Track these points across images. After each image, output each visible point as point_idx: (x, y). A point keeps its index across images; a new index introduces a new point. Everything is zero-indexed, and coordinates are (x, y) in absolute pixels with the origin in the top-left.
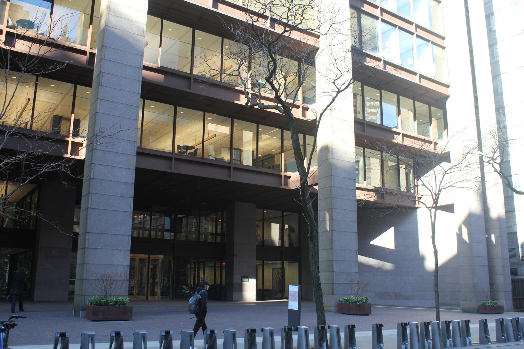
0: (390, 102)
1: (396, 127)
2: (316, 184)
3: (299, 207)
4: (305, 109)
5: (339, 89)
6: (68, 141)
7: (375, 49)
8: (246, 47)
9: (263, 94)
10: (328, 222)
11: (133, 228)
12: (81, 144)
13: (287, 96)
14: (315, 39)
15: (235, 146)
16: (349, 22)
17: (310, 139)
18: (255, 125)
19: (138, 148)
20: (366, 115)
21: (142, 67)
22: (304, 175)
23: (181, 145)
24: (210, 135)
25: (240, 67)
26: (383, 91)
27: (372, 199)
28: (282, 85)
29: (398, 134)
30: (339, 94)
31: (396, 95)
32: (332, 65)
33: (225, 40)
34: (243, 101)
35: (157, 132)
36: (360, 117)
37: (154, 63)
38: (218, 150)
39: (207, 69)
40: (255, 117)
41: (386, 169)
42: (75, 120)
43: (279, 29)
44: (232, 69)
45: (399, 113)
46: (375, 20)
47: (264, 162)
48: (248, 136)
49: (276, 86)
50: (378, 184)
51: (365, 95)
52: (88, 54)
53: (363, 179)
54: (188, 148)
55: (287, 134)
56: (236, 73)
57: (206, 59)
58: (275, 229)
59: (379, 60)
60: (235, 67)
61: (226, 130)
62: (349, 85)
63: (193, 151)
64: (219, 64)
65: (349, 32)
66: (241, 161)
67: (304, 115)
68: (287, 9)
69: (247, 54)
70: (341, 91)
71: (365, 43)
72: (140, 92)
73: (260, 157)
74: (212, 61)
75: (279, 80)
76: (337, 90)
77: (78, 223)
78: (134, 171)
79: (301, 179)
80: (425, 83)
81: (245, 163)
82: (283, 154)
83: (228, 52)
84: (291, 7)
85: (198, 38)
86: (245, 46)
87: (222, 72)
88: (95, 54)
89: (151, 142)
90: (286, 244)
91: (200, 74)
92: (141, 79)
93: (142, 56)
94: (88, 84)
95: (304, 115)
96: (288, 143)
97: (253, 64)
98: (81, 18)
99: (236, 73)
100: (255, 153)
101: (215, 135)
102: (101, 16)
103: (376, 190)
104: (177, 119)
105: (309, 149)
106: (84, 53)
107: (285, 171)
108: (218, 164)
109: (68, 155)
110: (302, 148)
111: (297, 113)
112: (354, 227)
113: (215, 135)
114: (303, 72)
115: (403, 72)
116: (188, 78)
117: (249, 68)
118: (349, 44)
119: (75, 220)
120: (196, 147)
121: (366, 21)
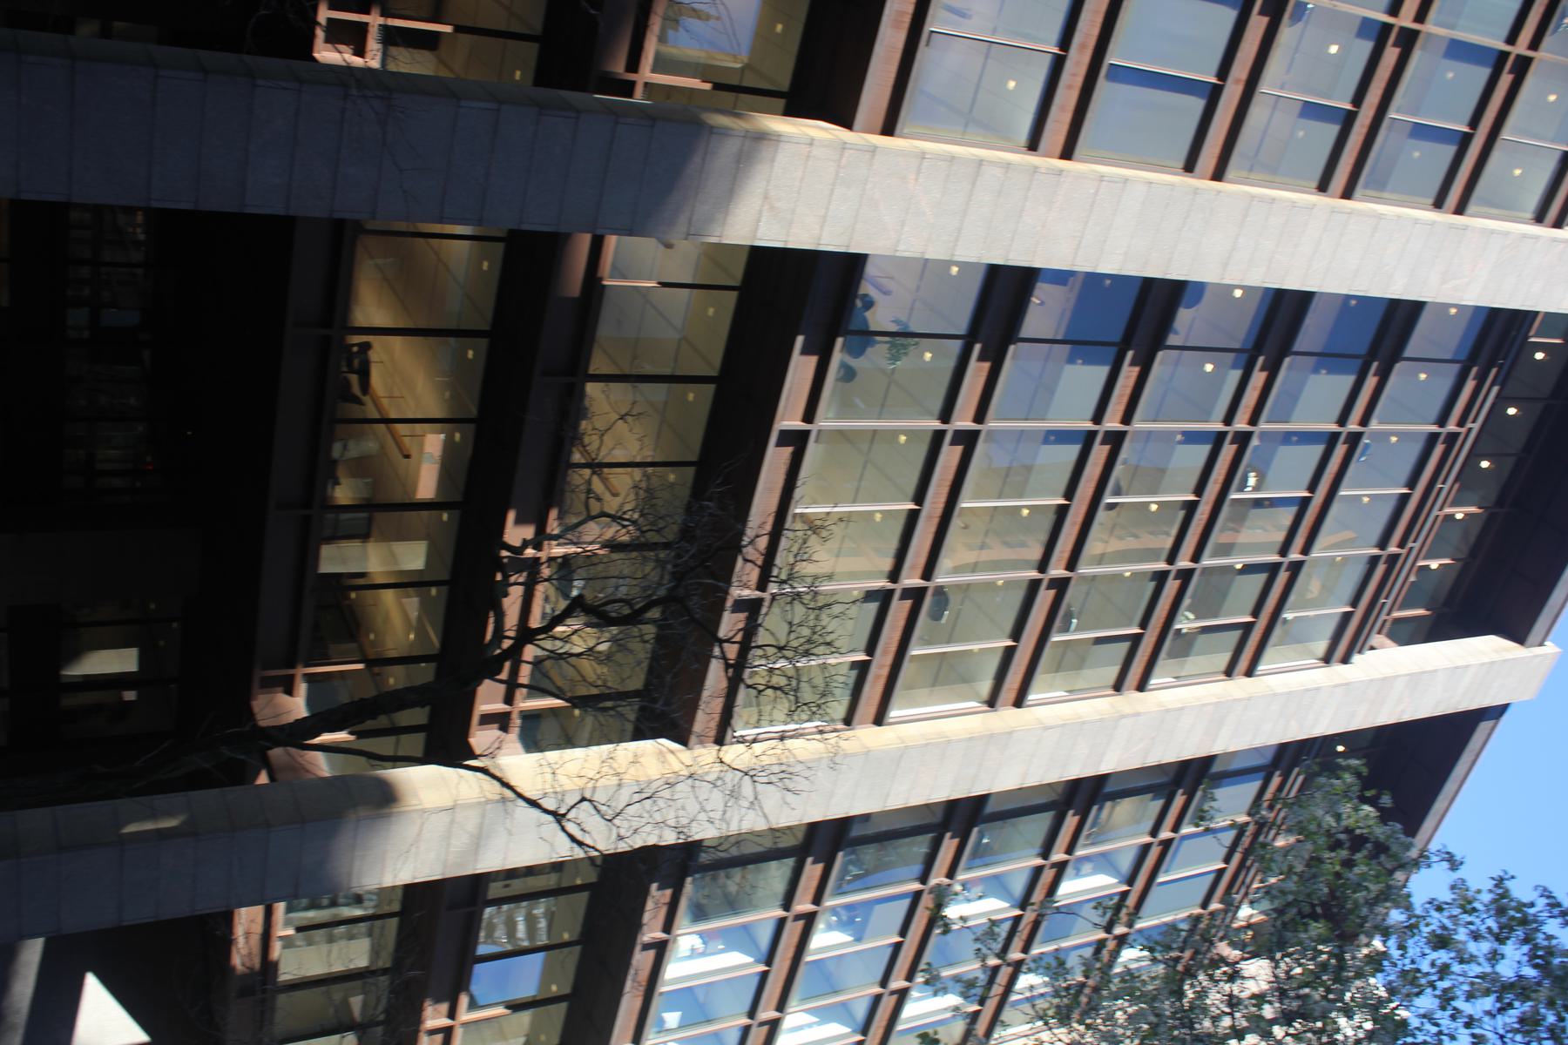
0: (547, 976)
1: (473, 1005)
2: (272, 778)
3: (197, 734)
4: (502, 721)
5: (564, 815)
6: (368, 13)
7: (700, 914)
8: (671, 534)
9: (541, 589)
10: (149, 826)
11: (98, 210)
12: (360, 52)
13: (537, 663)
14: (713, 733)
15: (380, 517)
16: (761, 826)
17: (415, 743)
18: (445, 576)
19: (359, 228)
20: (505, 907)
21: (599, 232)
22: (297, 735)
23: (373, 355)
24: (407, 440)
25: (614, 518)
26: (578, 949)
27: (237, 961)
28: (567, 648)
29: (452, 1014)
30: (550, 818)
31: (567, 990)
32: (631, 788)
33: (691, 471)
34: (516, 533)
35: (408, 282)
36: (495, 890)
37: (614, 267)
38: (361, 467)
39: (600, 423)
40: (470, 577)
41: (337, 992)
42: (436, 35)
43: (730, 624)
44: (607, 496)
45: (515, 1007)
46: (779, 901)
47: (337, 612)
48: (413, 556)
49: (559, 629)
50: (287, 973)
51: (562, 898)
52: (631, 77)
53: (305, 923)
54: (364, 374)
55: (425, 673)
56: (595, 508)
57: (629, 419)
58: (119, 661)
59: (668, 927)
60: (612, 505)
61: (427, 486)
62: (581, 844)
63: (356, 389)
64: (620, 455)
65: (734, 829)
66: (332, 538)
67: (487, 719)
68: (782, 643)
69: (653, 537)
70: (559, 822)
71: (714, 878)
72: (525, 227)
73: (348, 598)
74: (624, 437)
75: (578, 637)
76: (562, 811)
77: (106, 33)
78: (282, 212)
79: (282, 728)
80: (775, 459)
81: (327, 551)
82: (360, 666)
83: (655, 482)
84: (789, 654)
85: (691, 394)
86: (675, 528)
87: (596, 466)
88: (631, 96)
89: (380, 261)
90: (69, 701)
91: (587, 403)
92: (563, 229)
93: (631, 232)
94: (545, 76)
95: (487, 719)
96: (395, 679)
97: (622, 555)
98: (733, 55)
99: (595, 508)
100: (361, 582)
101: (408, 457)
102: (737, 116)
103: (269, 967)
104: (452, 340)
105: (384, 745)
106: (633, 66)
107: (310, 678)
108: (319, 471)
109: (324, 14)
110: (382, 721)
111: (489, 698)
112: (140, 913)
113: (408, 457)
114: (609, 704)
115: (638, 1003)
116: (574, 372)
117: (613, 546)
118: (703, 832)
119: (118, 25)
120: (366, 399)
121: (776, 875)
